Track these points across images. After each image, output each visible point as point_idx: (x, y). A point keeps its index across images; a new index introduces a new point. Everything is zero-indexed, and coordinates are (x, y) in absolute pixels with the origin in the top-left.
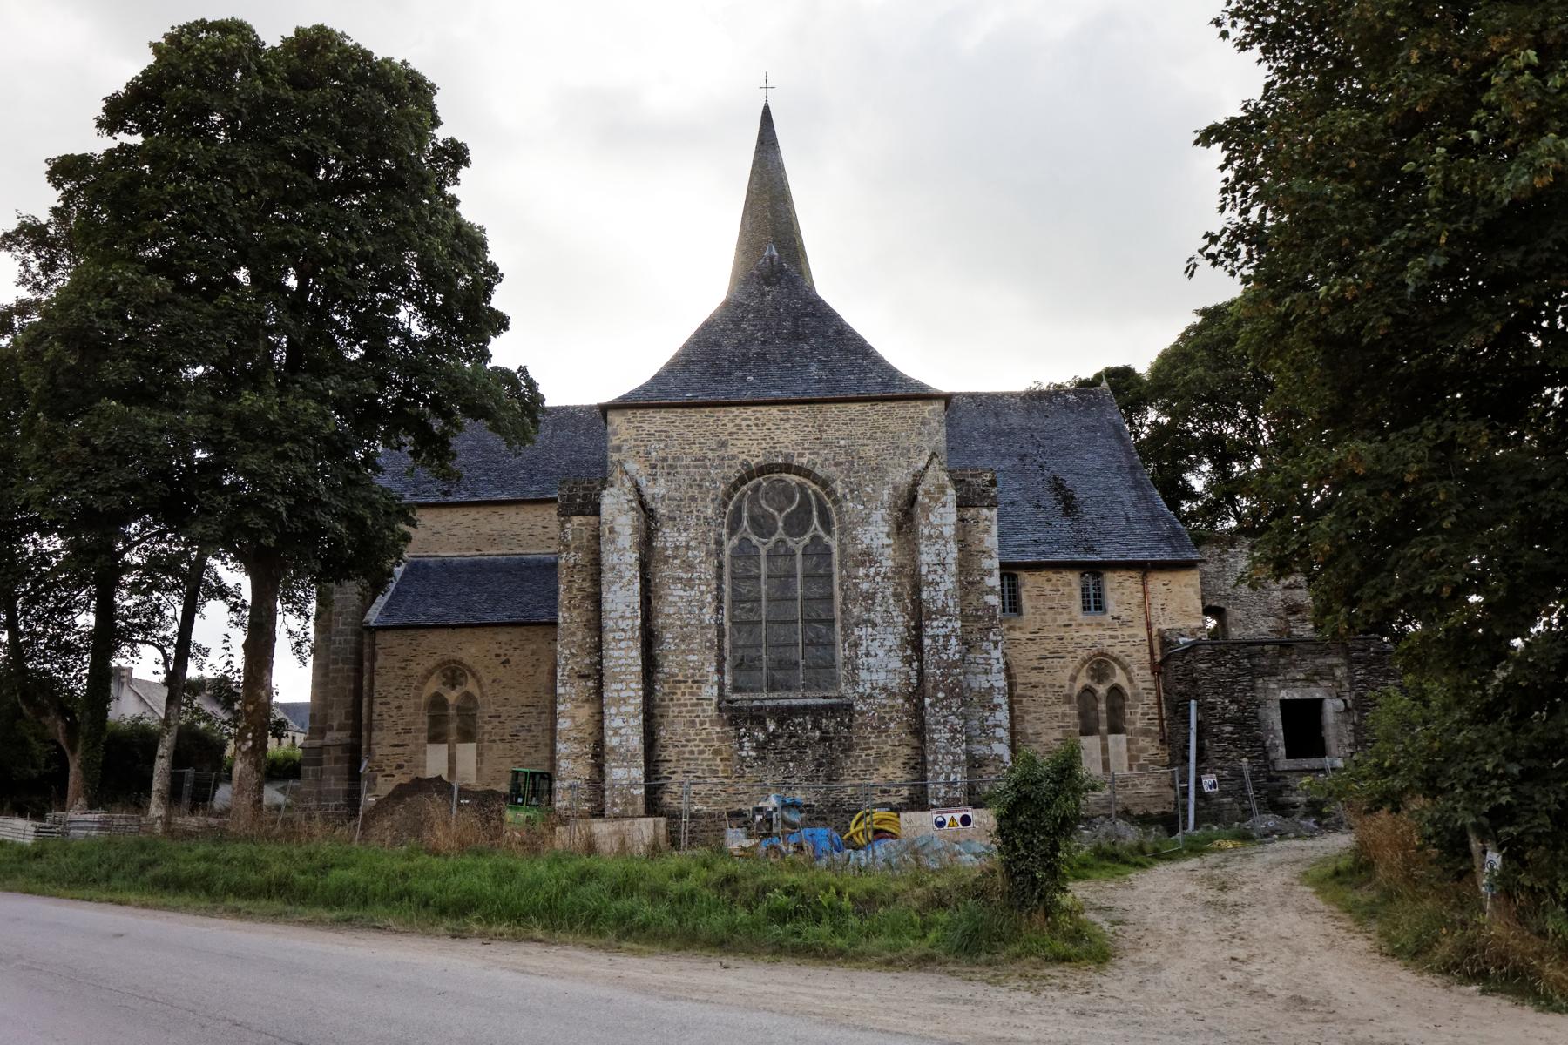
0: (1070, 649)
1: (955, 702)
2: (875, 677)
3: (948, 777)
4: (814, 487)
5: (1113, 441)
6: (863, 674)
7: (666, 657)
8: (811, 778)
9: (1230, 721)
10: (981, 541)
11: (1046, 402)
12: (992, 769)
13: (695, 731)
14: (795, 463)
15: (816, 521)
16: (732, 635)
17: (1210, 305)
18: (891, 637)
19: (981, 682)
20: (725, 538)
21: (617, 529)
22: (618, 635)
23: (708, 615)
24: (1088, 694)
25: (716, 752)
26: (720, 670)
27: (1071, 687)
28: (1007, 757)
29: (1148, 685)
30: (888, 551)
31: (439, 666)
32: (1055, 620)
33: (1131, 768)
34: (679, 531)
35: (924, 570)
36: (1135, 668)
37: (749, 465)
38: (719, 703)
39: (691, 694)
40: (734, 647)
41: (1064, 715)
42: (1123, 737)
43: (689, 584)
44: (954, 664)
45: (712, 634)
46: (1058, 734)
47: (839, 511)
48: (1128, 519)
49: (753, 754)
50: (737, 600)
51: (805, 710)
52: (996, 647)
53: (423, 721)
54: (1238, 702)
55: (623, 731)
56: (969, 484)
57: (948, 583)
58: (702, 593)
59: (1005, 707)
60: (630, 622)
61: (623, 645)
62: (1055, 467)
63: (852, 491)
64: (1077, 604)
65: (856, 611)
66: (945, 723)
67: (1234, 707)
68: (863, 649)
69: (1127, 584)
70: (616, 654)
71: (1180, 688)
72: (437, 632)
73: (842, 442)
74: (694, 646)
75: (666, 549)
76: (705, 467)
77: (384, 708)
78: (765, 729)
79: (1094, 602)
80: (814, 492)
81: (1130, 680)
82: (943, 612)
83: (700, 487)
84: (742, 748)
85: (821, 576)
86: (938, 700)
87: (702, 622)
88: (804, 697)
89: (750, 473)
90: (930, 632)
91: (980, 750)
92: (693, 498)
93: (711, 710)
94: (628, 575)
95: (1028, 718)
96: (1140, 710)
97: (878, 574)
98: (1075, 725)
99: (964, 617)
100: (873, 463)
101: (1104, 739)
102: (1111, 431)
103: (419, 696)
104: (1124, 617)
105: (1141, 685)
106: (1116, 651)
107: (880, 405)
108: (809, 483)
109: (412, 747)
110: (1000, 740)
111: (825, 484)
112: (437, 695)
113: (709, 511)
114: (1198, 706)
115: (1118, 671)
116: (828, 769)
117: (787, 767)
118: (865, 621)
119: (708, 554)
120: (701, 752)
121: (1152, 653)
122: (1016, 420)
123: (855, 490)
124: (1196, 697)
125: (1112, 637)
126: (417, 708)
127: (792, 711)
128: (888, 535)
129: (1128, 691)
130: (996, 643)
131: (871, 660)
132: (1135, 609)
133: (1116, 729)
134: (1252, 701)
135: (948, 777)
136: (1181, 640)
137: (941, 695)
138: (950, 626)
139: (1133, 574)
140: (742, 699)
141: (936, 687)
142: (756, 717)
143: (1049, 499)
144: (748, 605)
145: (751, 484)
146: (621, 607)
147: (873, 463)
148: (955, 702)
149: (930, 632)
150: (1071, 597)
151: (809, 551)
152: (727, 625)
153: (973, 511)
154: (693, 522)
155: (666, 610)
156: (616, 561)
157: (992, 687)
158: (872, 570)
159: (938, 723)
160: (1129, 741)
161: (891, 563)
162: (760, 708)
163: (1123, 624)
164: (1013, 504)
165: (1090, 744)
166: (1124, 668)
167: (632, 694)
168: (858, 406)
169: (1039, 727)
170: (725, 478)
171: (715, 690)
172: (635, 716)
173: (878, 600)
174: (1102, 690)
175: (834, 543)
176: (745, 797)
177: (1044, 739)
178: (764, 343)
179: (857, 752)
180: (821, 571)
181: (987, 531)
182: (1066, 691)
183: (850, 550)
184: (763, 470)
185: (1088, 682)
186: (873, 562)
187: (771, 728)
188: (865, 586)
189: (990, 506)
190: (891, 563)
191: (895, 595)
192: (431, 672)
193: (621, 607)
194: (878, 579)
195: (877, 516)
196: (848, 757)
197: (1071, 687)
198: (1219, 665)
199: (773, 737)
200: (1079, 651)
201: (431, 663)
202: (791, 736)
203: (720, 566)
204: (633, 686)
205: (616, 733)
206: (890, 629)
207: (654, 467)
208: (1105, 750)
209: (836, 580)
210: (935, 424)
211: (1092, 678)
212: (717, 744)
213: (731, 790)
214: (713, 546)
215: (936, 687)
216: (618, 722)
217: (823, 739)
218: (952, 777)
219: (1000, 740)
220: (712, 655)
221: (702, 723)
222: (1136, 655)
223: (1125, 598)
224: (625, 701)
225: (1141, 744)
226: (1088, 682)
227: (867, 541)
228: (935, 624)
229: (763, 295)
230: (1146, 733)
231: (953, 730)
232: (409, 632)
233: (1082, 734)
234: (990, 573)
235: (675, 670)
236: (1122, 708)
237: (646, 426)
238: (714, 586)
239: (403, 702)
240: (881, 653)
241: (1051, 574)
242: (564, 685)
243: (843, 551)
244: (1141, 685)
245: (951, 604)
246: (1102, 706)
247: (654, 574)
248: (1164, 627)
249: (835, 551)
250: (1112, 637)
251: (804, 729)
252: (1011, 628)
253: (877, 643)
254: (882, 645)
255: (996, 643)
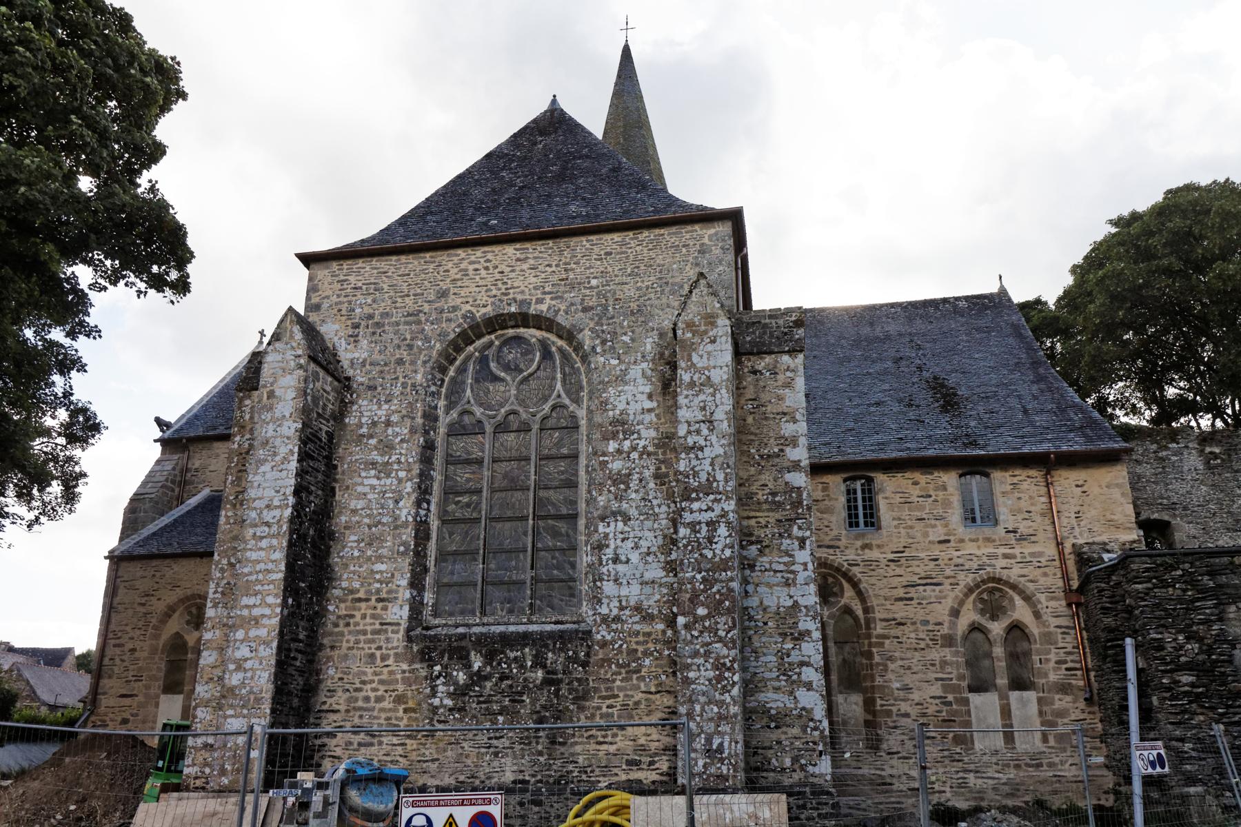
0: (948, 572)
1: (723, 622)
2: (624, 591)
3: (709, 740)
4: (560, 343)
5: (1011, 340)
6: (608, 588)
7: (346, 566)
8: (527, 740)
9: (1189, 667)
10: (780, 398)
11: (932, 310)
12: (796, 731)
13: (371, 668)
14: (532, 311)
15: (559, 386)
16: (440, 538)
17: (1126, 213)
18: (650, 535)
19: (777, 598)
20: (440, 412)
21: (277, 393)
22: (261, 530)
23: (406, 510)
24: (978, 636)
25: (400, 699)
26: (416, 583)
27: (953, 625)
28: (819, 712)
29: (1064, 622)
30: (649, 418)
31: (182, 601)
32: (926, 535)
33: (1045, 739)
34: (379, 403)
35: (682, 431)
36: (1042, 597)
37: (473, 317)
38: (409, 630)
39: (373, 616)
40: (442, 556)
41: (944, 663)
42: (1031, 695)
43: (384, 470)
44: (724, 565)
45: (408, 535)
46: (936, 690)
47: (589, 371)
48: (1025, 411)
49: (449, 702)
50: (450, 492)
51: (524, 639)
52: (802, 547)
53: (159, 666)
54: (1200, 640)
55: (248, 665)
56: (765, 326)
57: (717, 447)
58: (400, 481)
59: (817, 635)
60: (277, 513)
61: (264, 543)
62: (935, 368)
63: (604, 342)
64: (955, 516)
65: (602, 500)
66: (707, 654)
67: (1193, 647)
68: (609, 552)
69: (1025, 486)
70: (254, 556)
71: (1108, 621)
72: (184, 562)
73: (594, 282)
74: (384, 552)
75: (360, 425)
76: (419, 322)
77: (118, 651)
78: (468, 666)
79: (979, 515)
80: (560, 349)
81: (1037, 615)
82: (708, 488)
83: (410, 347)
84: (434, 694)
85: (565, 457)
86: (697, 619)
87: (396, 519)
88: (532, 623)
89: (474, 330)
90: (688, 517)
91: (775, 700)
92: (400, 362)
93: (397, 639)
94: (283, 451)
95: (891, 666)
96: (1053, 657)
97: (634, 449)
98: (961, 677)
99: (745, 501)
100: (634, 306)
101: (1004, 697)
102: (1009, 330)
103: (156, 637)
104: (1023, 528)
105: (1054, 622)
106: (1014, 574)
107: (646, 233)
108: (553, 338)
109: (141, 698)
110: (809, 686)
111: (569, 335)
112: (178, 635)
113: (419, 377)
114: (1137, 647)
115: (1018, 601)
116: (552, 723)
117: (494, 722)
118: (614, 514)
119: (413, 431)
120: (379, 699)
121: (1066, 577)
122: (892, 328)
123: (608, 341)
124: (1134, 634)
125: (1006, 556)
126: (154, 651)
127: (508, 641)
128: (650, 397)
129: (1034, 629)
130: (802, 541)
131: (621, 568)
132: (1039, 519)
133: (1019, 684)
134: (1221, 638)
135: (709, 740)
136: (1106, 556)
137: (701, 611)
138: (718, 511)
139: (1033, 473)
140: (443, 626)
141: (694, 600)
142: (458, 651)
143: (924, 396)
144: (465, 499)
145: (478, 343)
146: (270, 493)
147: (634, 306)
148: (723, 622)
149: (688, 517)
150: (947, 504)
151: (551, 423)
152: (434, 524)
153: (768, 359)
154: (397, 390)
155: (353, 504)
156: (271, 433)
157: (796, 605)
158: (627, 444)
159: (696, 654)
160: (1040, 701)
161: (653, 433)
162: (463, 637)
163: (1022, 539)
164: (878, 404)
165: (985, 706)
166: (1027, 598)
167: (267, 611)
168: (616, 237)
169: (909, 679)
170: (443, 334)
171: (405, 612)
172: (267, 643)
173: (633, 485)
174: (997, 628)
175: (582, 413)
176: (433, 767)
177: (916, 696)
178: (521, 188)
179: (596, 702)
180: (565, 451)
181: (788, 385)
182: (945, 630)
183: (598, 419)
184: (495, 323)
185: (976, 617)
186: (628, 433)
187: (476, 666)
188: (616, 465)
189: (792, 352)
190: (653, 433)
191: (657, 476)
192: (171, 610)
193: (270, 493)
194: (634, 455)
195: (635, 372)
196: (581, 709)
197: (953, 625)
198: (1164, 585)
199: (478, 678)
200: (961, 576)
201: (171, 597)
202: (503, 678)
203: (429, 446)
204: (270, 600)
205: (239, 668)
206: (648, 524)
207: (356, 326)
208: (1006, 712)
209: (583, 461)
210: (717, 251)
211: (982, 612)
212: (401, 687)
213: (414, 756)
214: (420, 421)
215: (694, 600)
216: (244, 652)
217: (547, 682)
218: (716, 742)
219: (809, 686)
220: (405, 564)
221: (384, 658)
222: (1042, 580)
223: (1024, 505)
224: (256, 621)
225: (1058, 705)
226: (976, 617)
227: (621, 406)
228: (696, 506)
229: (535, 144)
230: (1064, 688)
231: (719, 666)
232: (154, 563)
233: (972, 689)
234: (793, 442)
235: (356, 585)
236: (1028, 654)
237: (352, 278)
238: (416, 471)
239: (138, 644)
240: (635, 557)
241: (917, 476)
242: (215, 606)
243: (590, 420)
244: (1054, 622)
245: (720, 476)
246: (998, 651)
247: (342, 459)
248: (1081, 541)
249: (583, 422)
250: (1006, 556)
251: (522, 667)
252: (866, 546)
253: (629, 544)
254: (636, 547)
255: (802, 541)
